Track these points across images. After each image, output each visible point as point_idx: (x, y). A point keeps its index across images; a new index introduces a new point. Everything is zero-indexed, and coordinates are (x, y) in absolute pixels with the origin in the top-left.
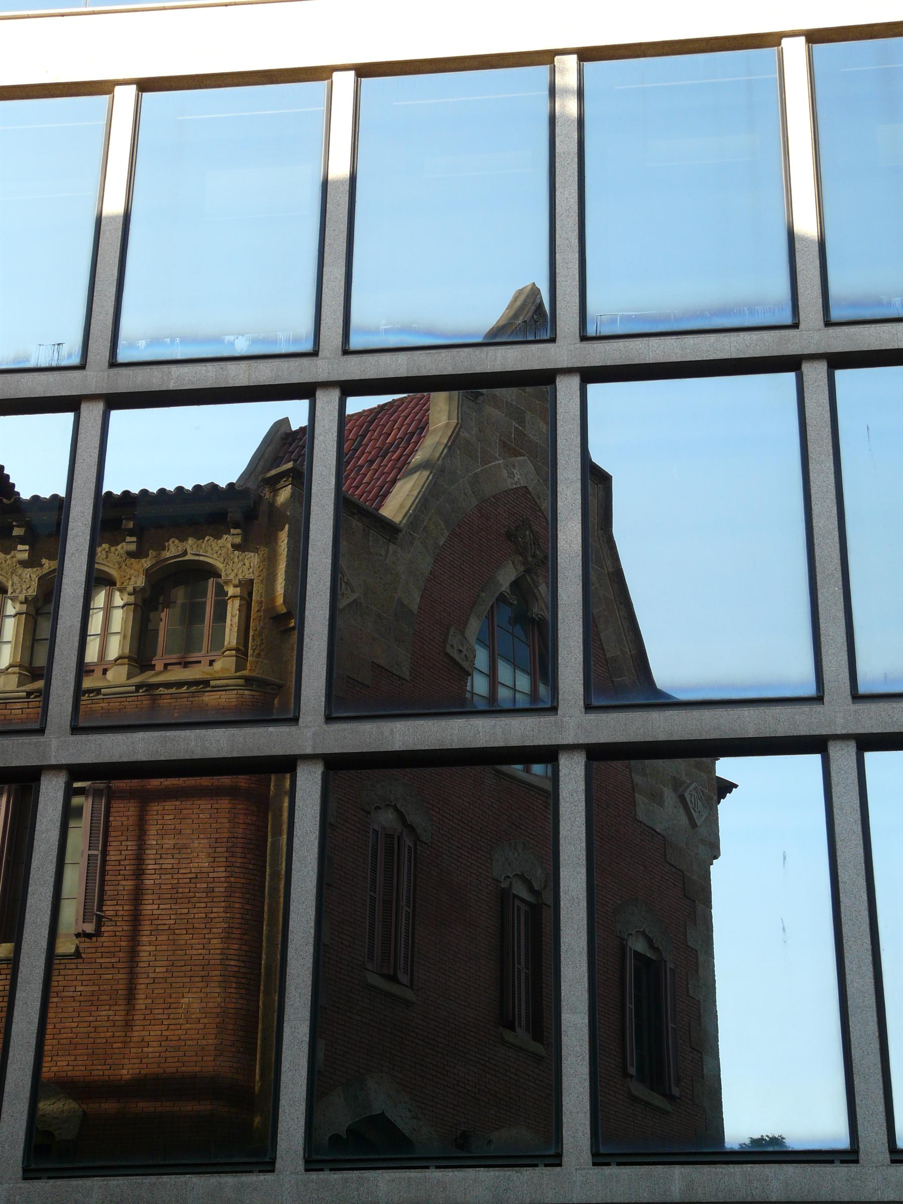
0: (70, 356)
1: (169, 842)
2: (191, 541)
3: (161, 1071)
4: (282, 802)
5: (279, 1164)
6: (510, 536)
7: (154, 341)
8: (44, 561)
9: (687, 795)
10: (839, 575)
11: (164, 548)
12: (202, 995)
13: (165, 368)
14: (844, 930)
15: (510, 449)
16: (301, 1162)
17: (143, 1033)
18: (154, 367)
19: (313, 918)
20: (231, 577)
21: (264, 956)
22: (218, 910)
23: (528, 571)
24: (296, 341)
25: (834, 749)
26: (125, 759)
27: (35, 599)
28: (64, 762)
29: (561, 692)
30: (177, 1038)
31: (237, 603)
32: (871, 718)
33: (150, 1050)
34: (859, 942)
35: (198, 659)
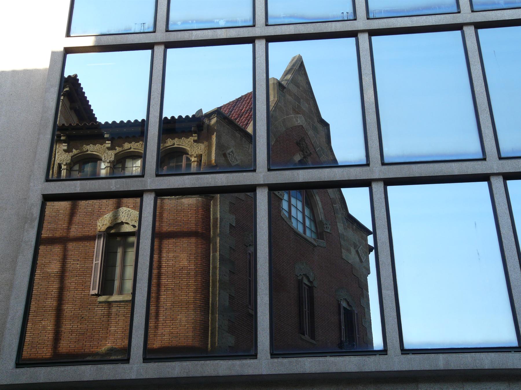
0: (148, 28)
1: (171, 255)
2: (176, 139)
4: (216, 240)
6: (298, 144)
7: (185, 22)
8: (116, 148)
10: (488, 109)
13: (190, 32)
14: (506, 254)
15: (297, 111)
16: (269, 355)
17: (162, 331)
19: (268, 252)
20: (193, 153)
21: (211, 300)
22: (192, 282)
23: (305, 157)
24: (245, 21)
25: (493, 179)
26: (180, 187)
27: (113, 162)
29: (370, 158)
31: (196, 163)
32: (509, 166)
33: (165, 337)
34: (513, 259)
35: (92, 297)
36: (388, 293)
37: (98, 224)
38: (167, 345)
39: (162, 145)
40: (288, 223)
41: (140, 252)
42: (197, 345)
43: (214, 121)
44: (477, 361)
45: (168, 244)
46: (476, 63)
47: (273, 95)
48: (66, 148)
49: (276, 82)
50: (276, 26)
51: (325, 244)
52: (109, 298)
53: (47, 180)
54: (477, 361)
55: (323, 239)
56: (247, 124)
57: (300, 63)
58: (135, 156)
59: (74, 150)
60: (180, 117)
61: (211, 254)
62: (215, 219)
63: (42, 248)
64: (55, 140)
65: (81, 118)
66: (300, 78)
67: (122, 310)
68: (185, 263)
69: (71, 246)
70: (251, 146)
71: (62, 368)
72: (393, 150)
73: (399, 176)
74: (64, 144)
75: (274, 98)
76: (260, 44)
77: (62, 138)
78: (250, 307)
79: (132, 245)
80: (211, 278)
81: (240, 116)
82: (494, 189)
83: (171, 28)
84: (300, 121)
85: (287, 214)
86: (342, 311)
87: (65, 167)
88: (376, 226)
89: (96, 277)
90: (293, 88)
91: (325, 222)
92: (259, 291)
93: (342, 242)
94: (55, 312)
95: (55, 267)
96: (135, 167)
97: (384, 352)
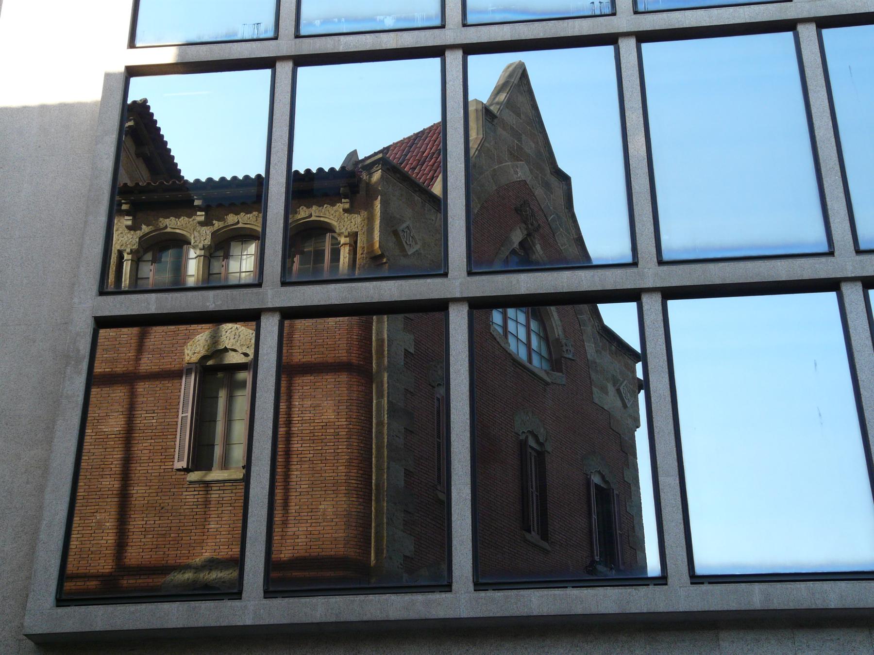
0: (266, 31)
1: (308, 403)
2: (314, 208)
3: (307, 554)
5: (455, 586)
6: (516, 210)
7: (326, 21)
8: (214, 222)
9: (621, 389)
10: (838, 168)
11: (296, 213)
12: (334, 503)
15: (516, 155)
18: (328, 38)
19: (468, 412)
20: (343, 230)
21: (374, 478)
22: (343, 447)
23: (529, 235)
24: (429, 18)
25: (846, 288)
26: (322, 303)
27: (210, 247)
28: (278, 305)
29: (639, 253)
30: (317, 532)
31: (347, 248)
33: (299, 540)
35: (178, 473)
36: (669, 481)
37: (186, 352)
38: (302, 553)
39: (290, 216)
40: (503, 345)
41: (256, 414)
42: (352, 553)
43: (377, 176)
44: (817, 596)
45: (303, 384)
46: (818, 88)
47: (475, 131)
48: (130, 223)
49: (480, 107)
50: (480, 28)
51: (564, 379)
52: (205, 475)
53: (102, 292)
54: (817, 596)
55: (562, 372)
56: (433, 179)
57: (521, 71)
58: (245, 236)
59: (144, 227)
60: (320, 170)
61: (374, 401)
62: (380, 341)
63: (94, 391)
64: (114, 211)
65: (153, 170)
66: (522, 99)
67: (227, 495)
68: (331, 416)
69: (142, 388)
70: (440, 216)
71: (132, 608)
72: (677, 238)
73: (688, 284)
74: (127, 218)
75: (478, 134)
76: (454, 58)
77: (125, 207)
78: (439, 488)
79: (243, 384)
80: (374, 441)
81: (421, 163)
82: (847, 305)
83: (303, 31)
84: (521, 172)
85: (500, 330)
86: (593, 491)
87: (130, 257)
88: (649, 368)
89: (183, 439)
90: (509, 118)
91: (564, 341)
92: (454, 478)
93: (593, 376)
94: (116, 500)
95: (115, 424)
96: (243, 263)
97: (662, 580)
